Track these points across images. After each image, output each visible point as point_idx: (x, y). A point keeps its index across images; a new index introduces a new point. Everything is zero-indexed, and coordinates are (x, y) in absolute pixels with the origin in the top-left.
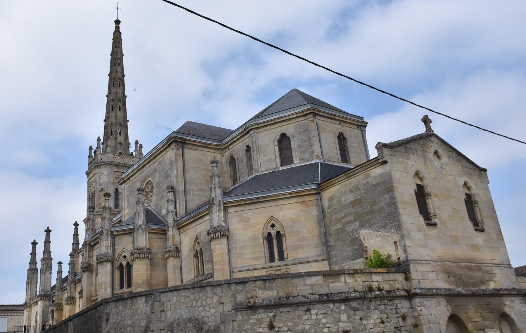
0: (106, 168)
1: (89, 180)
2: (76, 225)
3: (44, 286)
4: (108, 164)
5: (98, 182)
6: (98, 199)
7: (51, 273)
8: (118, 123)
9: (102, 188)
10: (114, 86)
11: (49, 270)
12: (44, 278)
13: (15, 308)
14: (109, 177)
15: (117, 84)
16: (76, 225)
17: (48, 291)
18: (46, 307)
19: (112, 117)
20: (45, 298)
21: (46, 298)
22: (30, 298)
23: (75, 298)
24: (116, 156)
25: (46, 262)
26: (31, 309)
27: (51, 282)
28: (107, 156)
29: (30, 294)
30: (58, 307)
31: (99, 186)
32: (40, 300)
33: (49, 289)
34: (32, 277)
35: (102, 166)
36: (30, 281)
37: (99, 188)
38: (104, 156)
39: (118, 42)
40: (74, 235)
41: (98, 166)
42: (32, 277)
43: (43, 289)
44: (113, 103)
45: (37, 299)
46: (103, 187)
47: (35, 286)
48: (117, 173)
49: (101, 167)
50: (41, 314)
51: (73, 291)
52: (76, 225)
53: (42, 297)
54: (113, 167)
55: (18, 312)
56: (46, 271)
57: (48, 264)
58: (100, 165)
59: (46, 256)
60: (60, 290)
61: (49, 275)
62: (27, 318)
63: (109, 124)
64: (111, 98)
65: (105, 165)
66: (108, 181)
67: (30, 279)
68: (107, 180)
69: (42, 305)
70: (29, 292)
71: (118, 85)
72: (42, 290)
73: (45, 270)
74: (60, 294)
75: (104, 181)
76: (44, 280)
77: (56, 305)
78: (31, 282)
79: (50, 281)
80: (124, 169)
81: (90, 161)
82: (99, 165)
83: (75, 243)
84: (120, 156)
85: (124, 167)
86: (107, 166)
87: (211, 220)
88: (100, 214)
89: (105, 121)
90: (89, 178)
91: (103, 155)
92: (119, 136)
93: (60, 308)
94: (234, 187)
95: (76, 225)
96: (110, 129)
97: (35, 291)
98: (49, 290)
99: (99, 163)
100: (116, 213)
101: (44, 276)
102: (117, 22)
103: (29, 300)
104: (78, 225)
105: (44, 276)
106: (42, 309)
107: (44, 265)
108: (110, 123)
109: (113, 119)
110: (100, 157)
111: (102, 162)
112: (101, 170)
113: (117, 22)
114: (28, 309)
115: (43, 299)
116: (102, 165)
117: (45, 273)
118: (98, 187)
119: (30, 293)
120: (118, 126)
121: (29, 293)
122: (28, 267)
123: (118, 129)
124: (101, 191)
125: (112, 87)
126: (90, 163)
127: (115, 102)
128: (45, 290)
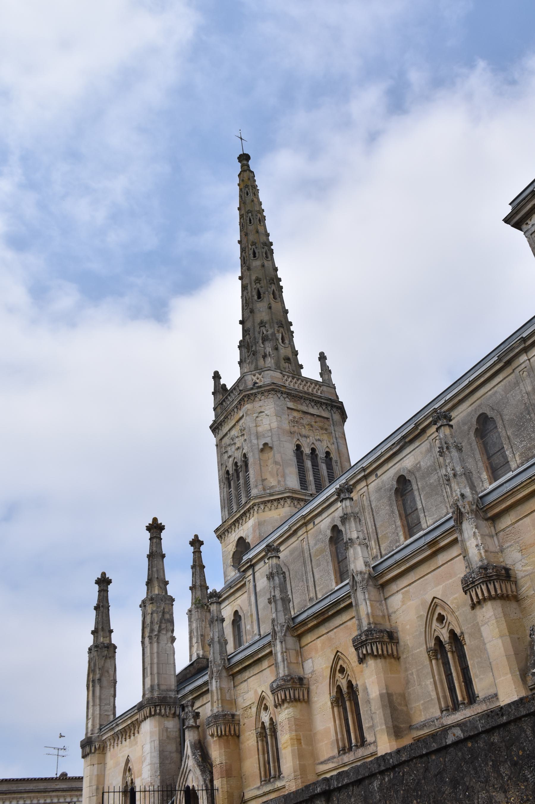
0: (272, 400)
1: (221, 439)
2: (197, 544)
3: (158, 673)
4: (273, 390)
5: (253, 430)
6: (259, 468)
7: (173, 639)
8: (275, 321)
9: (266, 444)
10: (255, 256)
11: (167, 631)
12: (158, 653)
13: (14, 787)
14: (279, 419)
15: (262, 253)
16: (197, 544)
17: (171, 691)
18: (168, 737)
19: (259, 311)
20: (163, 711)
21: (168, 710)
22: (101, 725)
23: (305, 681)
24: (286, 377)
25: (158, 607)
26: (104, 758)
27: (114, 707)
28: (268, 374)
29: (100, 715)
30: (225, 724)
31: (257, 439)
32: (151, 715)
33: (172, 682)
34: (103, 667)
35: (259, 396)
36: (98, 676)
37: (258, 444)
38: (260, 377)
39: (252, 186)
40: (193, 567)
41: (248, 396)
42: (103, 667)
43: (156, 682)
44: (258, 285)
45: (137, 717)
46: (268, 440)
47: (112, 692)
48: (293, 412)
49: (257, 399)
50: (157, 760)
51: (293, 660)
52: (196, 543)
53: (156, 706)
54: (285, 398)
55: (20, 796)
56: (159, 631)
57: (164, 613)
58: (255, 394)
59: (156, 592)
60: (224, 674)
61: (170, 645)
62: (94, 782)
63: (256, 324)
64: (254, 278)
65: (266, 394)
66: (278, 428)
67: (98, 671)
68: (274, 425)
69: (156, 730)
70: (97, 708)
71: (264, 255)
72: (152, 686)
73: (156, 627)
74: (225, 685)
75: (267, 427)
76: (158, 657)
77: (221, 721)
78: (99, 680)
79: (172, 662)
80: (307, 406)
81: (218, 400)
82: (252, 394)
83: (197, 587)
84: (295, 379)
85: (308, 402)
86: (270, 396)
87: (465, 554)
88: (268, 501)
89: (241, 322)
90: (220, 436)
91: (257, 375)
92: (282, 344)
93: (232, 728)
94: (495, 485)
95: (196, 543)
96: (259, 333)
97: (112, 704)
98: (173, 687)
99: (252, 389)
100: (307, 498)
101: (155, 645)
102: (244, 158)
103: (96, 731)
104: (202, 543)
105: (155, 645)
106: (157, 742)
107: (155, 615)
108: (258, 321)
109: (264, 314)
110: (250, 379)
111: (260, 387)
112: (257, 404)
113: (244, 158)
114: (96, 755)
115: (160, 714)
116: (258, 393)
117: (158, 636)
118: (255, 441)
119: (100, 710)
120: (276, 326)
121: (97, 712)
122: (90, 641)
123: (278, 331)
124: (262, 450)
125: (253, 258)
126: (222, 404)
127: (264, 283)
128: (163, 687)
